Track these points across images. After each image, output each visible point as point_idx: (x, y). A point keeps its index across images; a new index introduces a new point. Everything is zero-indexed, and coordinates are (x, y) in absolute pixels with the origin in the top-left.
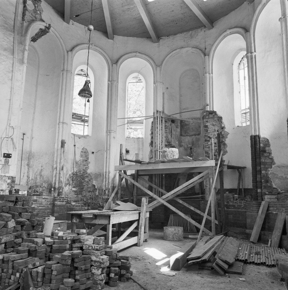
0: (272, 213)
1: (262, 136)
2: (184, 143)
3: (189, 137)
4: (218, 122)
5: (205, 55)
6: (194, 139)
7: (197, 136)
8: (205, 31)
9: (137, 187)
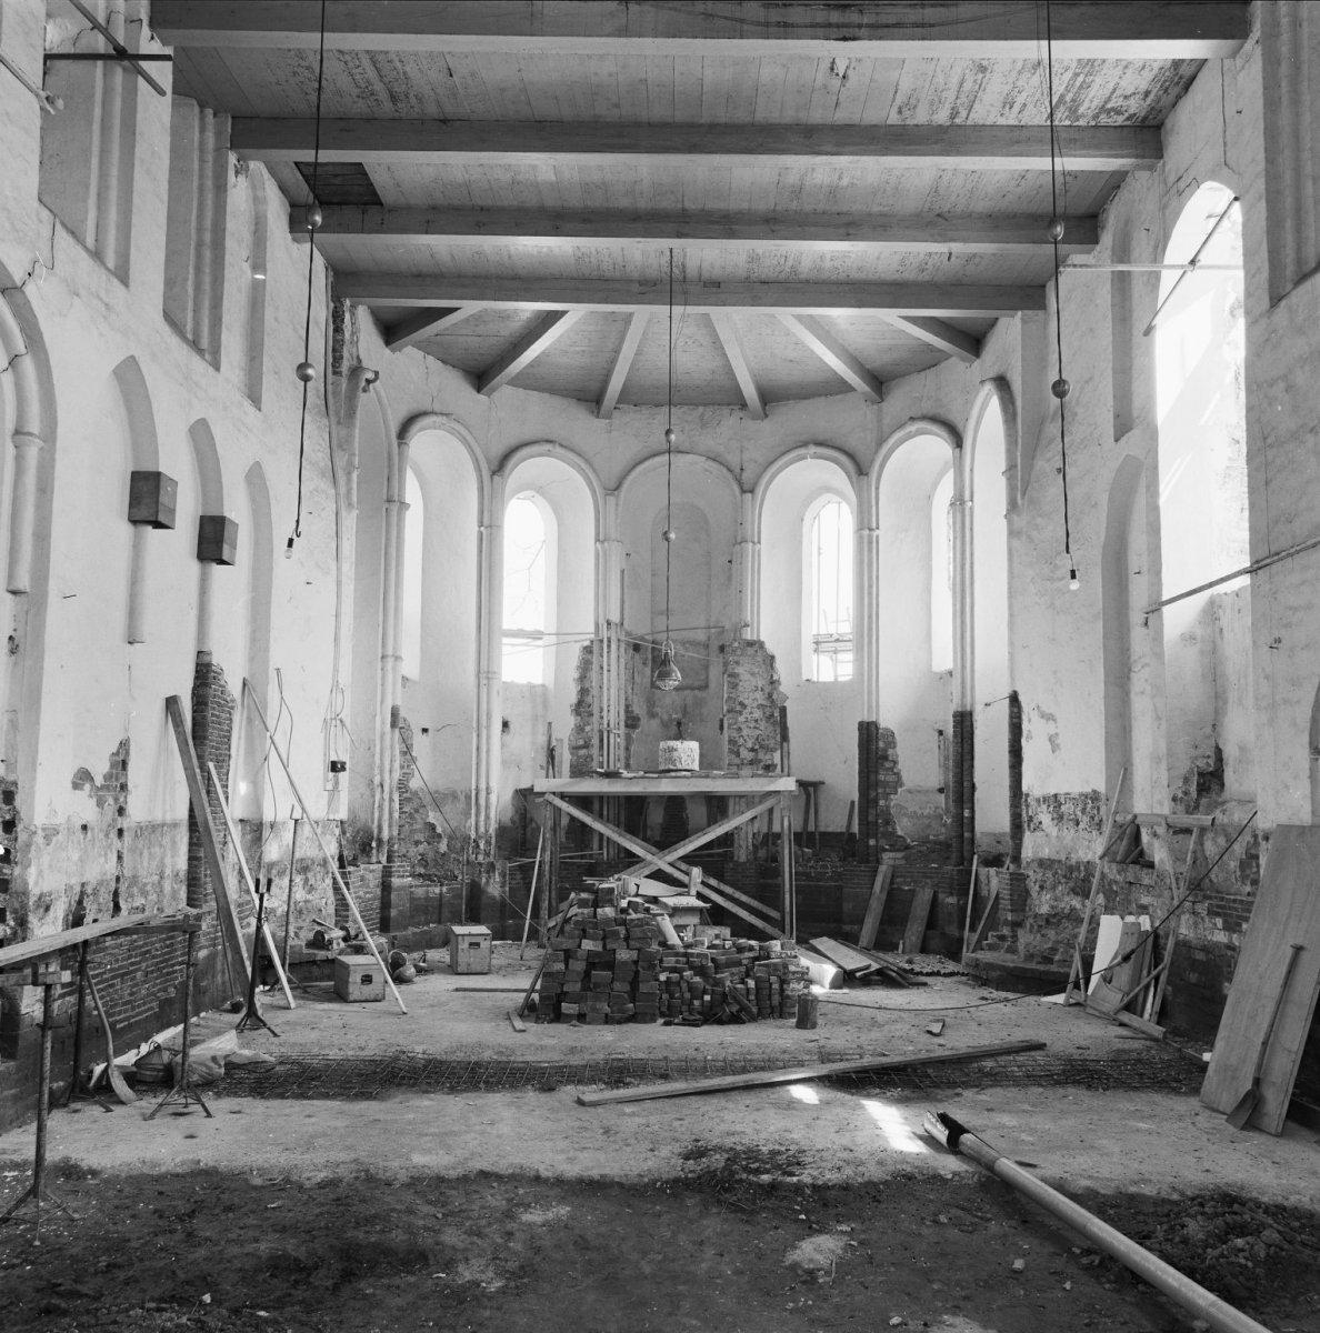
0: (900, 889)
1: (883, 724)
2: (661, 707)
4: (763, 666)
5: (743, 491)
6: (689, 701)
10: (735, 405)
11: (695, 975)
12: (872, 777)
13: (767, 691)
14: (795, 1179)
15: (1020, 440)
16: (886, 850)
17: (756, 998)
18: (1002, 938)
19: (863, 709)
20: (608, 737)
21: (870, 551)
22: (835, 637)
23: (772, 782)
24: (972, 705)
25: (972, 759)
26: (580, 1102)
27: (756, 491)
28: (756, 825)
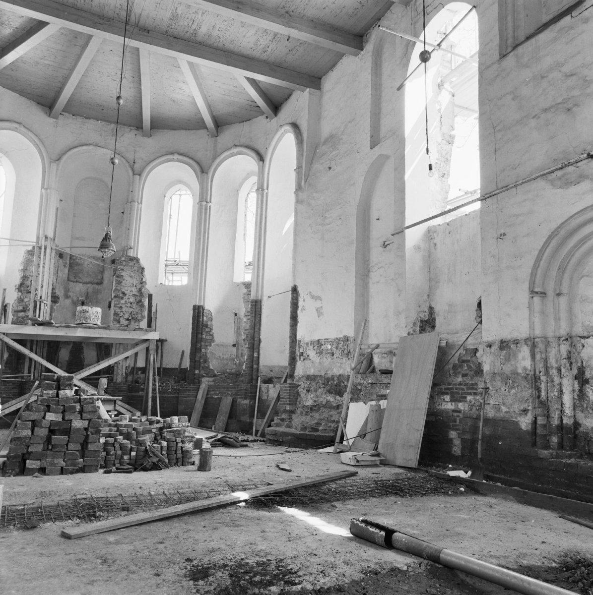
1: (207, 307)
2: (73, 292)
3: (81, 284)
5: (134, 174)
6: (90, 290)
7: (95, 286)
8: (136, 135)
9: (35, 361)
10: (133, 126)
11: (124, 439)
12: (200, 336)
13: (138, 287)
14: (299, 587)
15: (305, 154)
16: (204, 376)
17: (167, 453)
18: (283, 420)
19: (196, 298)
20: (40, 305)
21: (206, 213)
22: (177, 262)
23: (145, 334)
24: (262, 296)
25: (260, 325)
26: (66, 536)
27: (142, 175)
28: (128, 361)
